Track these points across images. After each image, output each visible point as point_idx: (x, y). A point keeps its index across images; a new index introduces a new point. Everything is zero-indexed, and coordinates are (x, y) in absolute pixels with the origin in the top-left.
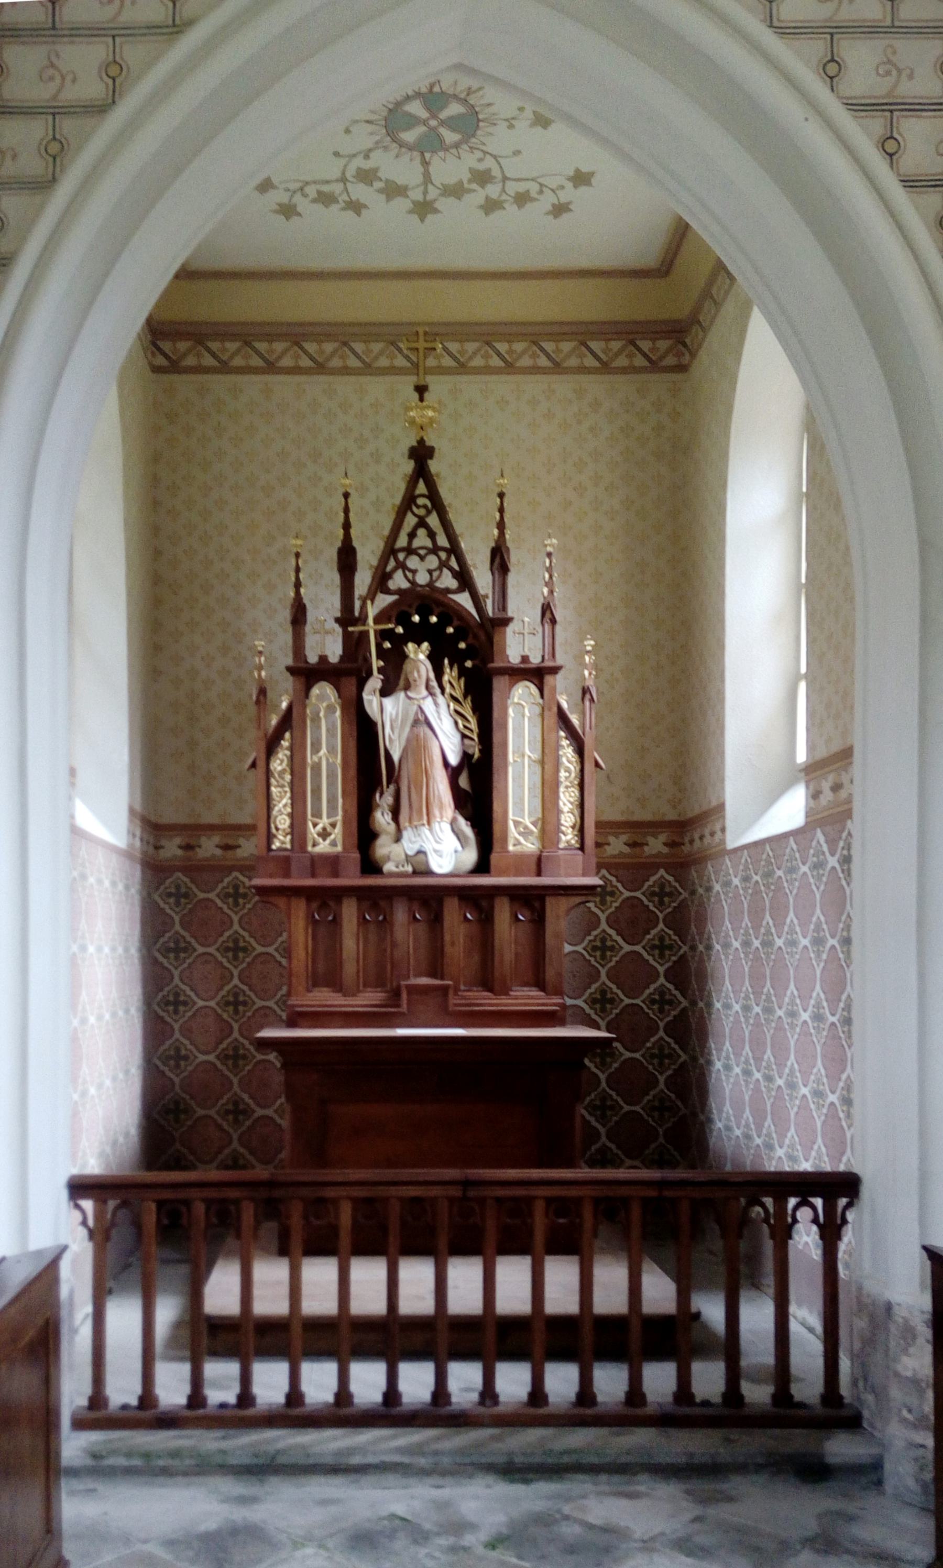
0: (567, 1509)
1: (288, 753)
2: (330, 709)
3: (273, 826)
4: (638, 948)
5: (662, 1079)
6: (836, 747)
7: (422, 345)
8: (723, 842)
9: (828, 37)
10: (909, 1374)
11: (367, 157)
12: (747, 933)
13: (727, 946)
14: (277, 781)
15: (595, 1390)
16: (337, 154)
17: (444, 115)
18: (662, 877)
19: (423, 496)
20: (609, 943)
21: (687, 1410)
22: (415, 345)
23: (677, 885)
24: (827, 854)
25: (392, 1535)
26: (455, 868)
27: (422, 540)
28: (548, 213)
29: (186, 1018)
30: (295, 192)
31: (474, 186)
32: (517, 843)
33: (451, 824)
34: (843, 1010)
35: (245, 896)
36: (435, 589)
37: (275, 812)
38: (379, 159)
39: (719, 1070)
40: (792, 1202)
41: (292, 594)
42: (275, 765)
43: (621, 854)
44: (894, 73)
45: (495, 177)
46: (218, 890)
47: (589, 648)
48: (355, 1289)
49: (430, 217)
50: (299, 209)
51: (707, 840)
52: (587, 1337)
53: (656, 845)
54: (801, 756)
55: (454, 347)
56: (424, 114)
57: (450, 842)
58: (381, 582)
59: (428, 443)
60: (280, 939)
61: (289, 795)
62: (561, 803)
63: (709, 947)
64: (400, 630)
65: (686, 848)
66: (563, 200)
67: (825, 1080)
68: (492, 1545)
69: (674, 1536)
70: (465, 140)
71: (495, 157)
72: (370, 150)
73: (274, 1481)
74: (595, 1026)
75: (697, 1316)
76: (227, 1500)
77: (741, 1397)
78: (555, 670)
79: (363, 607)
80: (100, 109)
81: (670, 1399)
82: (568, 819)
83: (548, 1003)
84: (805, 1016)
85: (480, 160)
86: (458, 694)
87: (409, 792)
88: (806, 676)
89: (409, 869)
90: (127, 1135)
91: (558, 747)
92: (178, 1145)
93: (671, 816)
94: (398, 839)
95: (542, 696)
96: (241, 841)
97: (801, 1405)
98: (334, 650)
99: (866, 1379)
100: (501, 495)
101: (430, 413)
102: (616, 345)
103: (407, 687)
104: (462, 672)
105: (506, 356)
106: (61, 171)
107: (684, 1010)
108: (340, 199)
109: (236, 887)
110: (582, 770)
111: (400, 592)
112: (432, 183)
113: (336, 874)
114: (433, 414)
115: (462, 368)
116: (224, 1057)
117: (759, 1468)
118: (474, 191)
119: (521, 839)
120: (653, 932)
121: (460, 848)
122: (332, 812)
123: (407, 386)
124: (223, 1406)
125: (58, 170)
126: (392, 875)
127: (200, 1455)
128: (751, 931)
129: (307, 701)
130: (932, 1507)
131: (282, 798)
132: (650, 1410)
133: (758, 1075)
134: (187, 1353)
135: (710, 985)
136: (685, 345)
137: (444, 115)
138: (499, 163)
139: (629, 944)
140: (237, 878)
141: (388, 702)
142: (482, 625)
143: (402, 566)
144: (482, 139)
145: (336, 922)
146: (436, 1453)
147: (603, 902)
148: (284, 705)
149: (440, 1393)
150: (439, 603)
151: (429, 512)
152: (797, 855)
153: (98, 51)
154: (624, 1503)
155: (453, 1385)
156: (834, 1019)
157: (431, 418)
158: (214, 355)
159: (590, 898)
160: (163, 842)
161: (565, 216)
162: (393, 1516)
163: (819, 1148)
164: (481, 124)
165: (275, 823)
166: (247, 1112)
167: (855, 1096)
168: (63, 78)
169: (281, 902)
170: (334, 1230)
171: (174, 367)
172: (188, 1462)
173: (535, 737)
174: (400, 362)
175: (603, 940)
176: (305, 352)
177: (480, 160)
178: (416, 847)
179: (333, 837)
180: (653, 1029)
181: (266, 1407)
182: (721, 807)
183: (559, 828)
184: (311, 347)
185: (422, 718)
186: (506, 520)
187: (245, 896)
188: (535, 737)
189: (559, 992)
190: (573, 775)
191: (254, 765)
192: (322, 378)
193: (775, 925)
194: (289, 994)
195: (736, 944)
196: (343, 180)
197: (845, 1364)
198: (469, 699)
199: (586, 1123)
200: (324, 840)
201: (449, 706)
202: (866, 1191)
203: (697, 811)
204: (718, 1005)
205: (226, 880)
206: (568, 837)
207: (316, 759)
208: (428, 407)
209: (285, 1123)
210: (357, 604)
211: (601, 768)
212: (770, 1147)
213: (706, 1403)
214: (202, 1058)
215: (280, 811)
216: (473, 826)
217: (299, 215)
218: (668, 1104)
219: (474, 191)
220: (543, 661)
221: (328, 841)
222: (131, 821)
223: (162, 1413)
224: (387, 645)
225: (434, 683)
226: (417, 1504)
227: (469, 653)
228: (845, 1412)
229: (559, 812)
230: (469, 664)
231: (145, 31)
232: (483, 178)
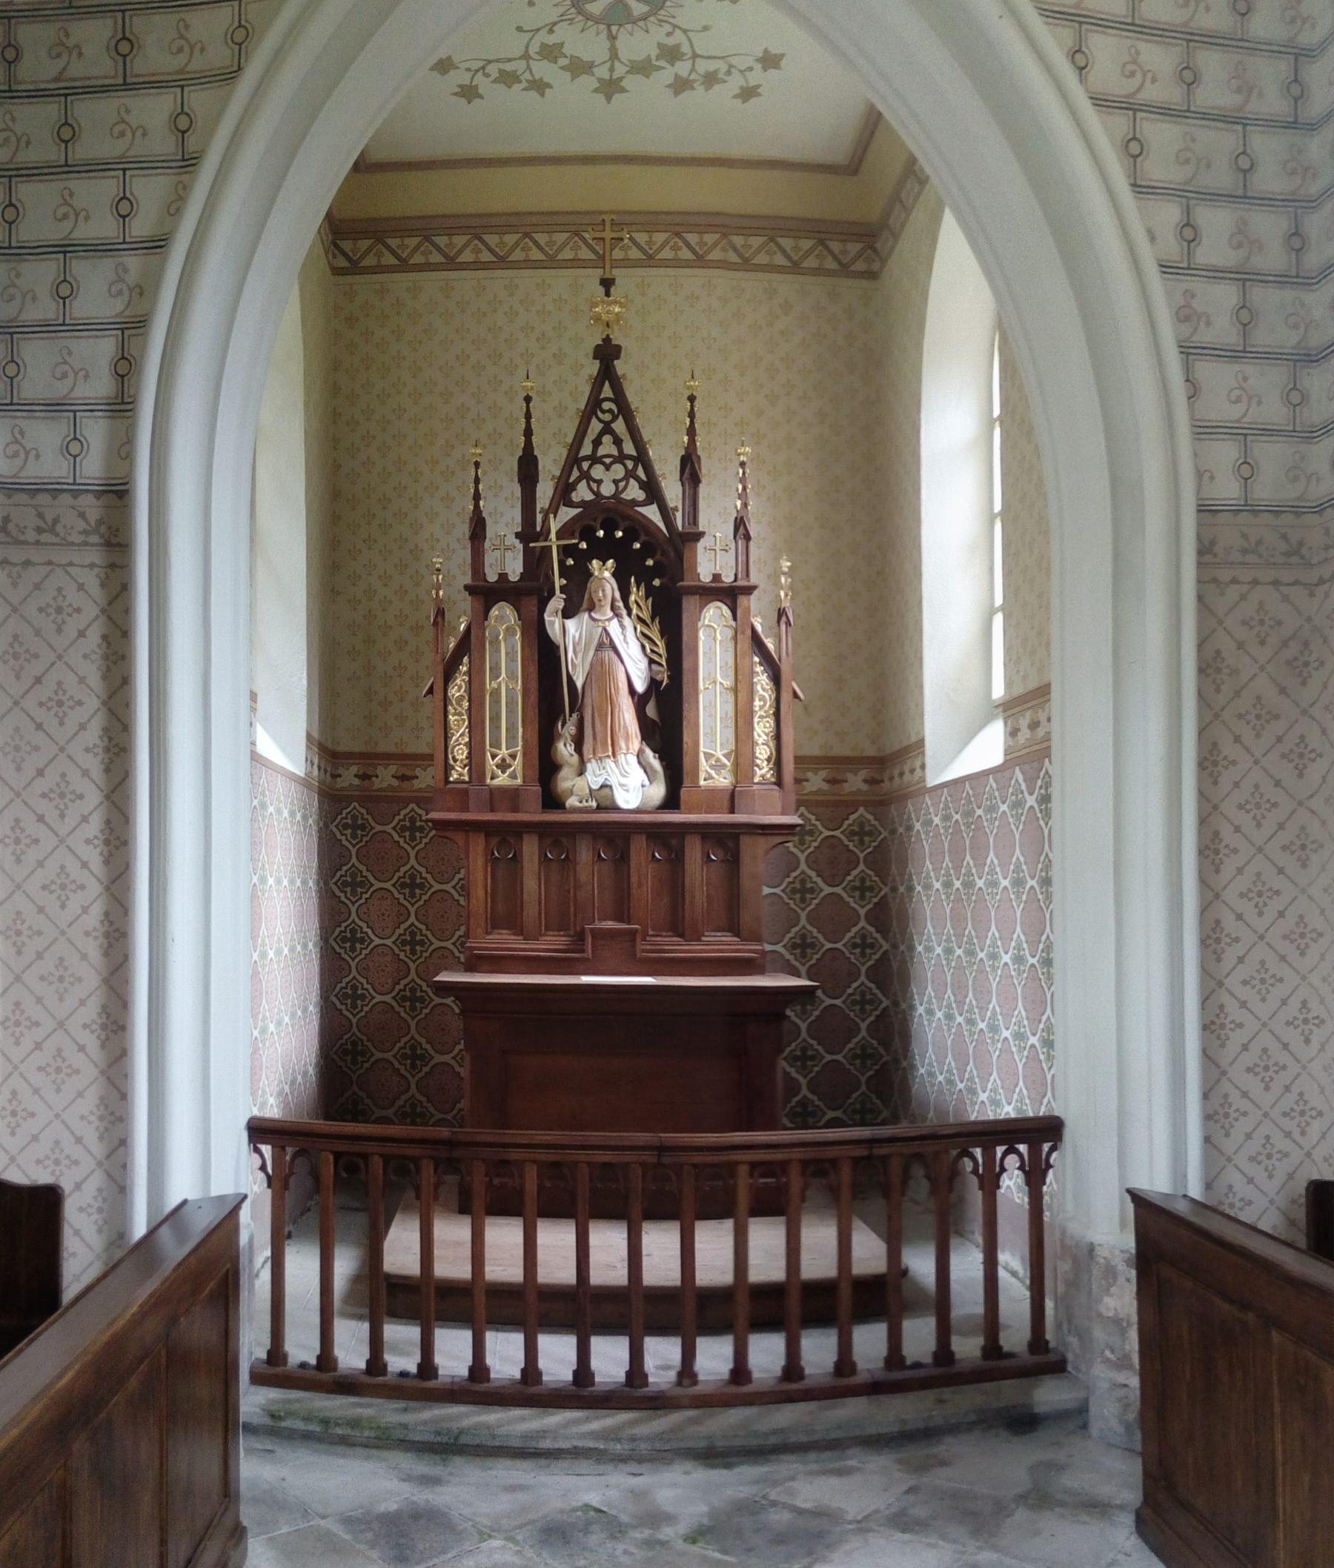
0: (773, 1495)
1: (467, 678)
2: (511, 632)
3: (450, 757)
4: (838, 890)
5: (864, 1026)
6: (1032, 684)
8: (923, 779)
10: (1111, 1314)
11: (551, 31)
12: (948, 874)
13: (928, 887)
14: (455, 709)
15: (803, 1363)
16: (519, 29)
18: (862, 815)
19: (607, 399)
21: (897, 1375)
22: (598, 235)
24: (1026, 793)
25: (586, 1530)
27: (607, 447)
28: (736, 97)
30: (477, 71)
31: (662, 63)
32: (709, 777)
33: (638, 756)
35: (421, 829)
36: (621, 501)
39: (921, 1015)
40: (1000, 1150)
42: (453, 691)
43: (819, 792)
45: (684, 54)
48: (541, 1255)
49: (617, 97)
51: (907, 777)
52: (794, 1304)
53: (855, 782)
54: (998, 691)
55: (642, 238)
57: (638, 775)
58: (564, 493)
60: (458, 877)
61: (466, 723)
63: (911, 889)
64: (584, 545)
65: (886, 785)
67: (1026, 1022)
68: (692, 1539)
69: (887, 1512)
70: (653, 13)
71: (685, 31)
72: (555, 24)
73: (458, 1461)
74: (796, 974)
75: (905, 1272)
76: (408, 1478)
77: (952, 1354)
78: (749, 590)
79: (546, 520)
81: (881, 1364)
82: (763, 752)
83: (747, 950)
84: (1006, 958)
85: (669, 34)
86: (646, 615)
88: (1002, 608)
89: (594, 804)
90: (305, 1074)
91: (752, 673)
92: (355, 1088)
93: (871, 751)
94: (581, 772)
95: (735, 619)
96: (418, 771)
97: (1010, 1355)
98: (514, 568)
99: (1069, 1323)
100: (692, 399)
102: (806, 244)
103: (591, 608)
107: (886, 952)
109: (413, 820)
110: (778, 700)
111: (583, 504)
112: (618, 59)
113: (515, 809)
115: (650, 260)
116: (401, 999)
117: (970, 1427)
118: (664, 68)
119: (713, 773)
120: (854, 873)
121: (647, 782)
122: (511, 741)
123: (590, 279)
124: (404, 1374)
126: (575, 810)
127: (379, 1427)
128: (952, 872)
129: (486, 623)
130: (1139, 1447)
132: (860, 1378)
133: (960, 1019)
134: (366, 1311)
135: (912, 929)
136: (875, 250)
138: (690, 40)
139: (830, 886)
141: (571, 624)
142: (670, 540)
143: (586, 476)
144: (671, 10)
145: (517, 859)
146: (633, 1439)
149: (636, 1372)
150: (626, 517)
151: (615, 418)
152: (997, 793)
154: (834, 1481)
155: (650, 1364)
156: (1034, 961)
159: (790, 838)
160: (341, 771)
161: (753, 101)
162: (587, 1507)
163: (1021, 1090)
165: (452, 753)
166: (424, 1058)
167: (1058, 1038)
169: (459, 837)
170: (520, 1192)
172: (367, 1433)
173: (727, 664)
174: (585, 254)
175: (803, 882)
177: (669, 34)
178: (601, 781)
180: (854, 975)
181: (449, 1380)
182: (921, 743)
183: (753, 761)
185: (607, 641)
186: (696, 425)
187: (421, 829)
188: (727, 664)
189: (758, 938)
191: (431, 691)
193: (975, 866)
194: (467, 935)
195: (937, 885)
196: (526, 56)
197: (1049, 1305)
198: (657, 620)
199: (786, 1074)
200: (503, 772)
201: (635, 629)
202: (1068, 1134)
203: (897, 747)
204: (920, 948)
206: (763, 770)
207: (494, 685)
209: (464, 1072)
210: (539, 518)
212: (973, 1092)
213: (917, 1365)
216: (661, 759)
217: (481, 97)
218: (870, 1051)
219: (664, 68)
220: (736, 580)
223: (340, 1376)
224: (570, 562)
225: (621, 604)
226: (613, 1494)
227: (658, 570)
228: (1052, 1357)
229: (753, 744)
230: (657, 582)
232: (672, 54)
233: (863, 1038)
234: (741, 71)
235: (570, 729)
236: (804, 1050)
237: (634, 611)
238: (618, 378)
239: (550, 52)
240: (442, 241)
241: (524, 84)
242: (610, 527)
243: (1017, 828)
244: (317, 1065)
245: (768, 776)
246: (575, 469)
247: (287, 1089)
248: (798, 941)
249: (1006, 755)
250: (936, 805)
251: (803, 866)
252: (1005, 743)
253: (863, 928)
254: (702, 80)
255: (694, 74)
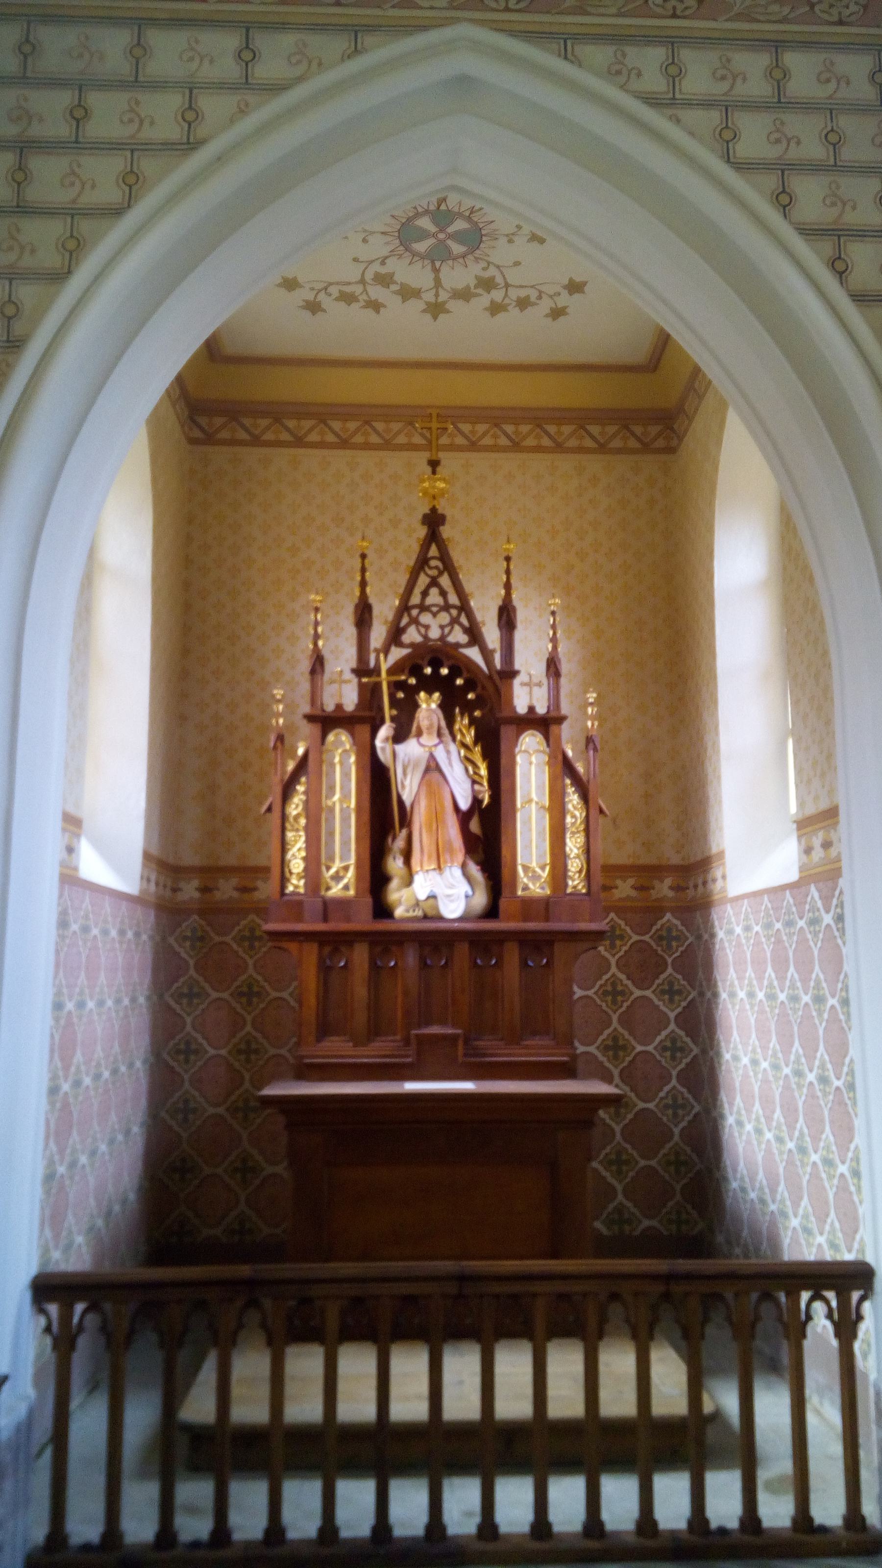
1: (303, 797)
3: (287, 870)
6: (824, 805)
7: (434, 425)
9: (780, 172)
11: (383, 263)
12: (750, 985)
13: (732, 995)
14: (292, 826)
16: (356, 260)
17: (450, 230)
19: (433, 558)
20: (620, 988)
22: (428, 425)
23: (683, 928)
26: (466, 911)
27: (434, 597)
28: (547, 316)
29: (196, 1068)
30: (320, 291)
31: (479, 291)
34: (847, 1074)
35: (260, 938)
37: (289, 856)
38: (392, 265)
40: (805, 1296)
41: (311, 646)
43: (628, 898)
44: (839, 204)
45: (498, 284)
46: (234, 934)
47: (591, 700)
49: (442, 317)
50: (323, 306)
56: (433, 229)
58: (395, 636)
59: (440, 511)
61: (303, 839)
62: (567, 849)
65: (691, 893)
66: (559, 306)
71: (498, 267)
72: (386, 258)
74: (607, 1078)
78: (560, 720)
80: (117, 212)
85: (484, 269)
86: (469, 740)
87: (421, 835)
90: (124, 1202)
94: (409, 881)
95: (548, 745)
96: (259, 884)
101: (442, 485)
102: (611, 429)
103: (419, 734)
104: (473, 721)
105: (586, 435)
106: (77, 264)
108: (360, 298)
111: (412, 645)
112: (442, 287)
114: (444, 485)
115: (473, 446)
123: (421, 460)
125: (73, 262)
131: (296, 841)
136: (672, 429)
137: (450, 230)
138: (502, 273)
140: (253, 921)
143: (415, 621)
147: (613, 946)
148: (301, 751)
150: (449, 657)
151: (441, 573)
152: (794, 909)
153: (117, 163)
157: (442, 489)
158: (247, 430)
160: (182, 884)
161: (562, 319)
164: (484, 238)
168: (83, 185)
169: (293, 947)
171: (209, 439)
176: (330, 428)
177: (484, 269)
179: (345, 881)
180: (665, 1078)
184: (336, 425)
185: (433, 765)
190: (579, 821)
191: (269, 809)
192: (348, 452)
194: (298, 1044)
196: (362, 281)
203: (699, 858)
205: (243, 923)
208: (439, 479)
211: (606, 815)
214: (211, 1110)
215: (293, 855)
217: (324, 311)
221: (341, 885)
222: (144, 865)
224: (401, 695)
225: (446, 731)
230: (477, 713)
231: (160, 147)
232: (487, 284)
233: (677, 1144)
234: (551, 297)
235: (400, 843)
236: (619, 1153)
237: (459, 737)
238: (443, 541)
239: (384, 280)
240: (291, 424)
241: (362, 303)
242: (436, 664)
243: (816, 945)
244: (141, 1189)
245: (580, 887)
246: (406, 615)
247: (100, 1223)
248: (611, 1053)
249: (801, 872)
250: (737, 915)
251: (614, 969)
252: (800, 860)
253: (670, 975)
254: (514, 304)
255: (507, 298)
